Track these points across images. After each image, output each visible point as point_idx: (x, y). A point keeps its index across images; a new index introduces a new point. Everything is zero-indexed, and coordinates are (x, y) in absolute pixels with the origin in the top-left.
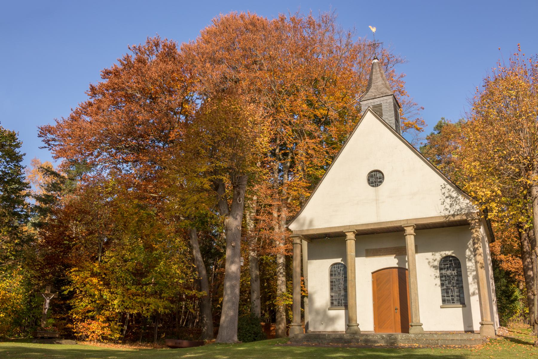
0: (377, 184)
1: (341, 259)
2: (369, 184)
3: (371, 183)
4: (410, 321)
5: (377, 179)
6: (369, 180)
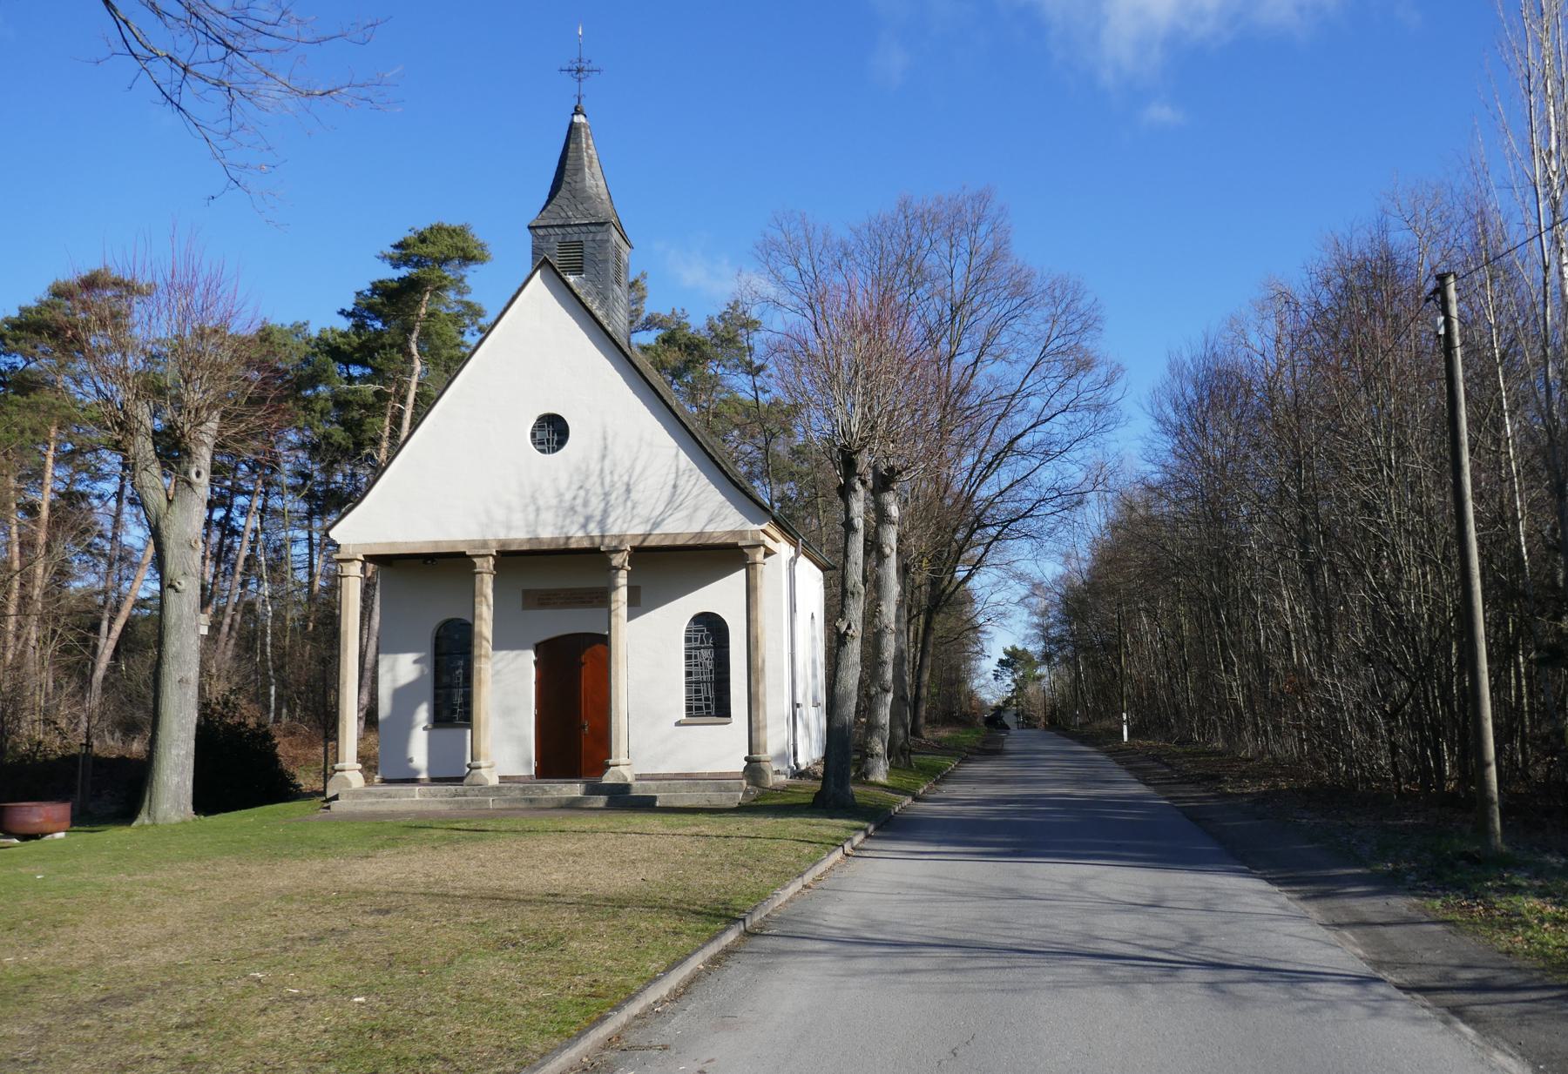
6: (533, 435)
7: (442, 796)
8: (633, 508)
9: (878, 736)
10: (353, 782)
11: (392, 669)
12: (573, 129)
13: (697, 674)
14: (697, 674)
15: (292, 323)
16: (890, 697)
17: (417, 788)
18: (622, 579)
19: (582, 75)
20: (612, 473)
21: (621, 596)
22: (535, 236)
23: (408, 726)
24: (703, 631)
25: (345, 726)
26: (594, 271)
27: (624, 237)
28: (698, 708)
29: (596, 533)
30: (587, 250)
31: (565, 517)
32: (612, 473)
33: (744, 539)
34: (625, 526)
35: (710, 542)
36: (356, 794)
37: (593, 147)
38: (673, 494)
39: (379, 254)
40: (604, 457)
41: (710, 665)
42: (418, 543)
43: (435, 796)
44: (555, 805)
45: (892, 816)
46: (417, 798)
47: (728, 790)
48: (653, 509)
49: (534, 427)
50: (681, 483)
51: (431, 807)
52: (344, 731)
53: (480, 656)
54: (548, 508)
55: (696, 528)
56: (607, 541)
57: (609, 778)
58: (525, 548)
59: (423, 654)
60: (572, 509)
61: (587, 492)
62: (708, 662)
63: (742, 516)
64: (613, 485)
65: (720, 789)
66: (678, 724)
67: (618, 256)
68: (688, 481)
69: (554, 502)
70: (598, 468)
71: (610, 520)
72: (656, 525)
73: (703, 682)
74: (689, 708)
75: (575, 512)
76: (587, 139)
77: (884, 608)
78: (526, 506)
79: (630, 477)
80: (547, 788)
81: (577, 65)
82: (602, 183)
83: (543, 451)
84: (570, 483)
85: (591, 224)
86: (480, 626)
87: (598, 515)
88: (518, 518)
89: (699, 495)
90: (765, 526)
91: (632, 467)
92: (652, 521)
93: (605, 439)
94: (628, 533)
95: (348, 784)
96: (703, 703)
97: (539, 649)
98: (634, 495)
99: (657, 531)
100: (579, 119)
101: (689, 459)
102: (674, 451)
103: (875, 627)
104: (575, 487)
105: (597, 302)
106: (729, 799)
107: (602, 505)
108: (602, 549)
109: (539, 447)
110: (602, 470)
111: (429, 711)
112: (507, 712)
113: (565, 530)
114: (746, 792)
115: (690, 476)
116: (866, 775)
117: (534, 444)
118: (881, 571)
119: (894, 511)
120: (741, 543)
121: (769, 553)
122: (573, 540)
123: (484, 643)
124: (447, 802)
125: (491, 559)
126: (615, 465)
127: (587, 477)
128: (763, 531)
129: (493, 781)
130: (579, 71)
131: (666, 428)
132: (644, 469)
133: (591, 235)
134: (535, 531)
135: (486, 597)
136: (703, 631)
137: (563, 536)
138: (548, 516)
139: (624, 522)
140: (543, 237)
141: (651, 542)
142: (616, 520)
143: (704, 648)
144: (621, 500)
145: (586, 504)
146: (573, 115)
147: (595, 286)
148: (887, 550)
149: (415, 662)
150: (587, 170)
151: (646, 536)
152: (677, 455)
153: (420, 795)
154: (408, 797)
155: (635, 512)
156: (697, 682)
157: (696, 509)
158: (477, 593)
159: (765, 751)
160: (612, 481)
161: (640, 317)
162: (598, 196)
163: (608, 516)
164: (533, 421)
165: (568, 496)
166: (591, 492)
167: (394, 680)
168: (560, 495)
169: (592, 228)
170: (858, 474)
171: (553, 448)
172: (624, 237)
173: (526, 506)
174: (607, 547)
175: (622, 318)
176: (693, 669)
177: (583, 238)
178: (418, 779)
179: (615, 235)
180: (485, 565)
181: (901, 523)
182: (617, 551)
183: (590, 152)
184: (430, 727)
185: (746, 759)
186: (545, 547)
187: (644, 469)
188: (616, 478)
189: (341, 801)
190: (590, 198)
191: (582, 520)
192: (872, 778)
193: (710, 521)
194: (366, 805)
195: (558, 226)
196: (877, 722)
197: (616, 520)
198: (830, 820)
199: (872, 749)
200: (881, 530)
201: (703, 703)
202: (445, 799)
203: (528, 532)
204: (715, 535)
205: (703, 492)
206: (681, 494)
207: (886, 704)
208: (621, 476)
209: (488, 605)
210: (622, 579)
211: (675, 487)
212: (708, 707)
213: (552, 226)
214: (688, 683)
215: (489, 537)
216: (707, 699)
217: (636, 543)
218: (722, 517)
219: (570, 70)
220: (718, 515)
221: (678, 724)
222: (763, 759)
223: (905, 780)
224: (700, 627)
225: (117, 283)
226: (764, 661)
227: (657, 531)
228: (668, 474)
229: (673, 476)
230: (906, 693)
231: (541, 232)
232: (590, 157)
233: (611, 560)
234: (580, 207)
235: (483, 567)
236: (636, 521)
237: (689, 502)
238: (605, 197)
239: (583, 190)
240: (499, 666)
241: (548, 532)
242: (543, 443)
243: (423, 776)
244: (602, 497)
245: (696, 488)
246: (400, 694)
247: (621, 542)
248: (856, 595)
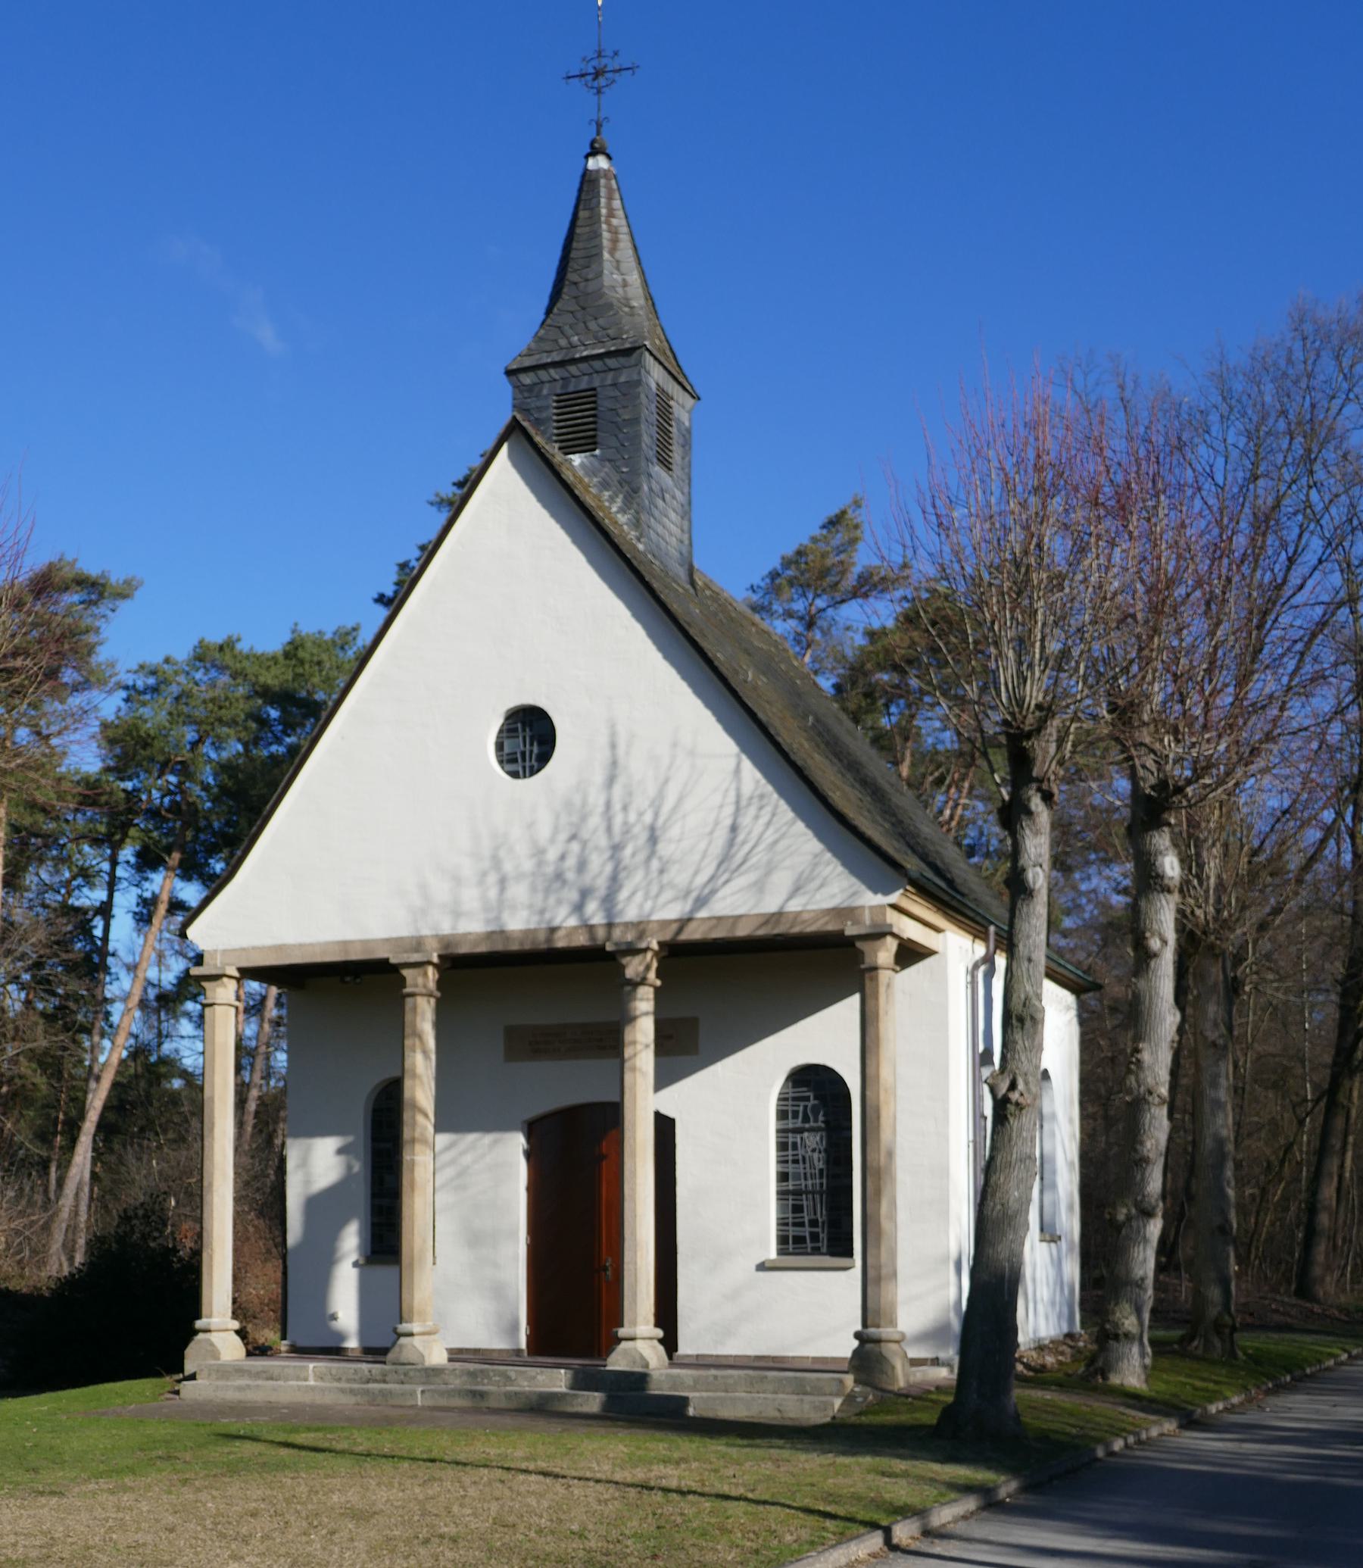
6: (499, 747)
7: (348, 1381)
8: (662, 871)
9: (1129, 1301)
10: (222, 1352)
11: (304, 1163)
12: (588, 182)
13: (797, 1177)
14: (797, 1177)
15: (334, 629)
16: (1155, 1228)
17: (311, 1366)
18: (644, 1003)
19: (602, 81)
20: (625, 808)
21: (643, 1032)
22: (518, 387)
23: (327, 1261)
24: (807, 1099)
25: (211, 1257)
26: (614, 442)
27: (678, 377)
28: (799, 1240)
29: (598, 919)
30: (604, 404)
31: (547, 891)
32: (625, 808)
33: (857, 922)
34: (648, 905)
35: (796, 930)
36: (226, 1372)
37: (621, 213)
38: (731, 843)
39: (433, 498)
40: (611, 781)
41: (819, 1162)
42: (320, 944)
43: (339, 1380)
44: (513, 1405)
45: (1097, 1460)
46: (312, 1383)
47: (818, 1391)
48: (696, 873)
49: (501, 731)
50: (746, 821)
51: (328, 1399)
52: (211, 1266)
53: (413, 1141)
54: (520, 877)
55: (770, 906)
56: (617, 933)
57: (618, 1362)
58: (483, 948)
59: (350, 1139)
60: (559, 876)
61: (584, 844)
62: (816, 1155)
63: (853, 880)
64: (627, 829)
65: (801, 1390)
66: (762, 1267)
67: (665, 411)
68: (757, 817)
69: (528, 865)
70: (601, 801)
71: (623, 895)
72: (701, 902)
73: (807, 1192)
74: (782, 1240)
75: (564, 882)
76: (610, 198)
77: (1146, 1056)
78: (484, 874)
79: (656, 815)
80: (513, 1375)
81: (595, 63)
82: (634, 278)
83: (515, 775)
84: (556, 830)
85: (609, 354)
86: (413, 1088)
87: (602, 884)
88: (470, 898)
89: (776, 842)
90: (895, 897)
91: (660, 796)
92: (694, 895)
93: (613, 746)
94: (656, 917)
95: (214, 1353)
96: (806, 1231)
97: (534, 1130)
98: (664, 849)
99: (703, 914)
100: (599, 163)
101: (758, 775)
102: (732, 763)
103: (1129, 1091)
104: (563, 836)
105: (619, 500)
106: (816, 1408)
107: (609, 868)
108: (609, 947)
109: (511, 767)
110: (608, 805)
111: (361, 1233)
112: (476, 1239)
113: (547, 916)
114: (850, 1399)
115: (761, 808)
116: (1104, 1373)
117: (501, 762)
118: (1142, 984)
119: (1171, 866)
120: (850, 930)
121: (910, 954)
122: (560, 934)
123: (420, 1118)
124: (352, 1391)
125: (430, 970)
126: (630, 794)
127: (584, 818)
128: (894, 907)
129: (436, 1356)
130: (597, 74)
131: (720, 720)
132: (680, 800)
133: (611, 375)
134: (498, 918)
135: (420, 1038)
136: (807, 1099)
137: (544, 926)
138: (519, 892)
139: (646, 897)
140: (530, 388)
141: (692, 933)
142: (633, 893)
143: (811, 1130)
144: (641, 857)
145: (582, 866)
146: (587, 157)
147: (617, 469)
148: (1155, 944)
149: (340, 1151)
150: (606, 255)
151: (684, 922)
152: (737, 771)
153: (320, 1377)
154: (298, 1379)
155: (666, 878)
156: (797, 1193)
157: (769, 870)
158: (408, 1030)
159: (893, 1322)
160: (625, 823)
161: (849, 575)
162: (626, 302)
163: (621, 887)
164: (497, 722)
165: (552, 855)
166: (590, 845)
167: (307, 1182)
168: (539, 853)
169: (611, 362)
170: (1040, 781)
171: (532, 767)
172: (678, 377)
173: (484, 874)
174: (616, 944)
175: (673, 528)
176: (791, 1168)
177: (596, 384)
178: (345, 1349)
179: (655, 375)
180: (420, 980)
181: (1184, 888)
182: (633, 951)
183: (614, 222)
184: (361, 1262)
185: (858, 1335)
186: (515, 947)
187: (680, 800)
188: (632, 817)
189: (199, 1382)
190: (610, 306)
191: (574, 896)
192: (1115, 1380)
193: (791, 896)
194: (230, 1392)
195: (555, 364)
196: (1128, 1271)
197: (633, 893)
198: (936, 1467)
199: (1116, 1325)
200: (1143, 904)
201: (806, 1231)
202: (356, 1386)
203: (488, 921)
204: (806, 916)
205: (782, 837)
206: (744, 843)
207: (1146, 1240)
208: (641, 814)
209: (425, 1052)
210: (644, 1003)
211: (734, 829)
212: (815, 1237)
213: (544, 366)
214: (782, 1194)
215: (426, 932)
216: (814, 1223)
217: (667, 936)
218: (817, 882)
219: (583, 75)
220: (810, 879)
221: (762, 1267)
222: (884, 1336)
223: (1176, 1382)
224: (804, 1092)
225: (83, 582)
226: (890, 1154)
227: (703, 914)
228: (721, 806)
229: (730, 809)
230: (1227, 1221)
231: (527, 379)
232: (614, 231)
233: (623, 967)
234: (593, 325)
235: (416, 986)
236: (668, 895)
237: (759, 857)
238: (638, 302)
239: (599, 293)
240: (467, 1159)
241: (519, 921)
242: (515, 761)
243: (352, 1343)
244: (607, 854)
245: (771, 830)
246: (314, 1204)
247: (641, 936)
248: (1028, 1023)
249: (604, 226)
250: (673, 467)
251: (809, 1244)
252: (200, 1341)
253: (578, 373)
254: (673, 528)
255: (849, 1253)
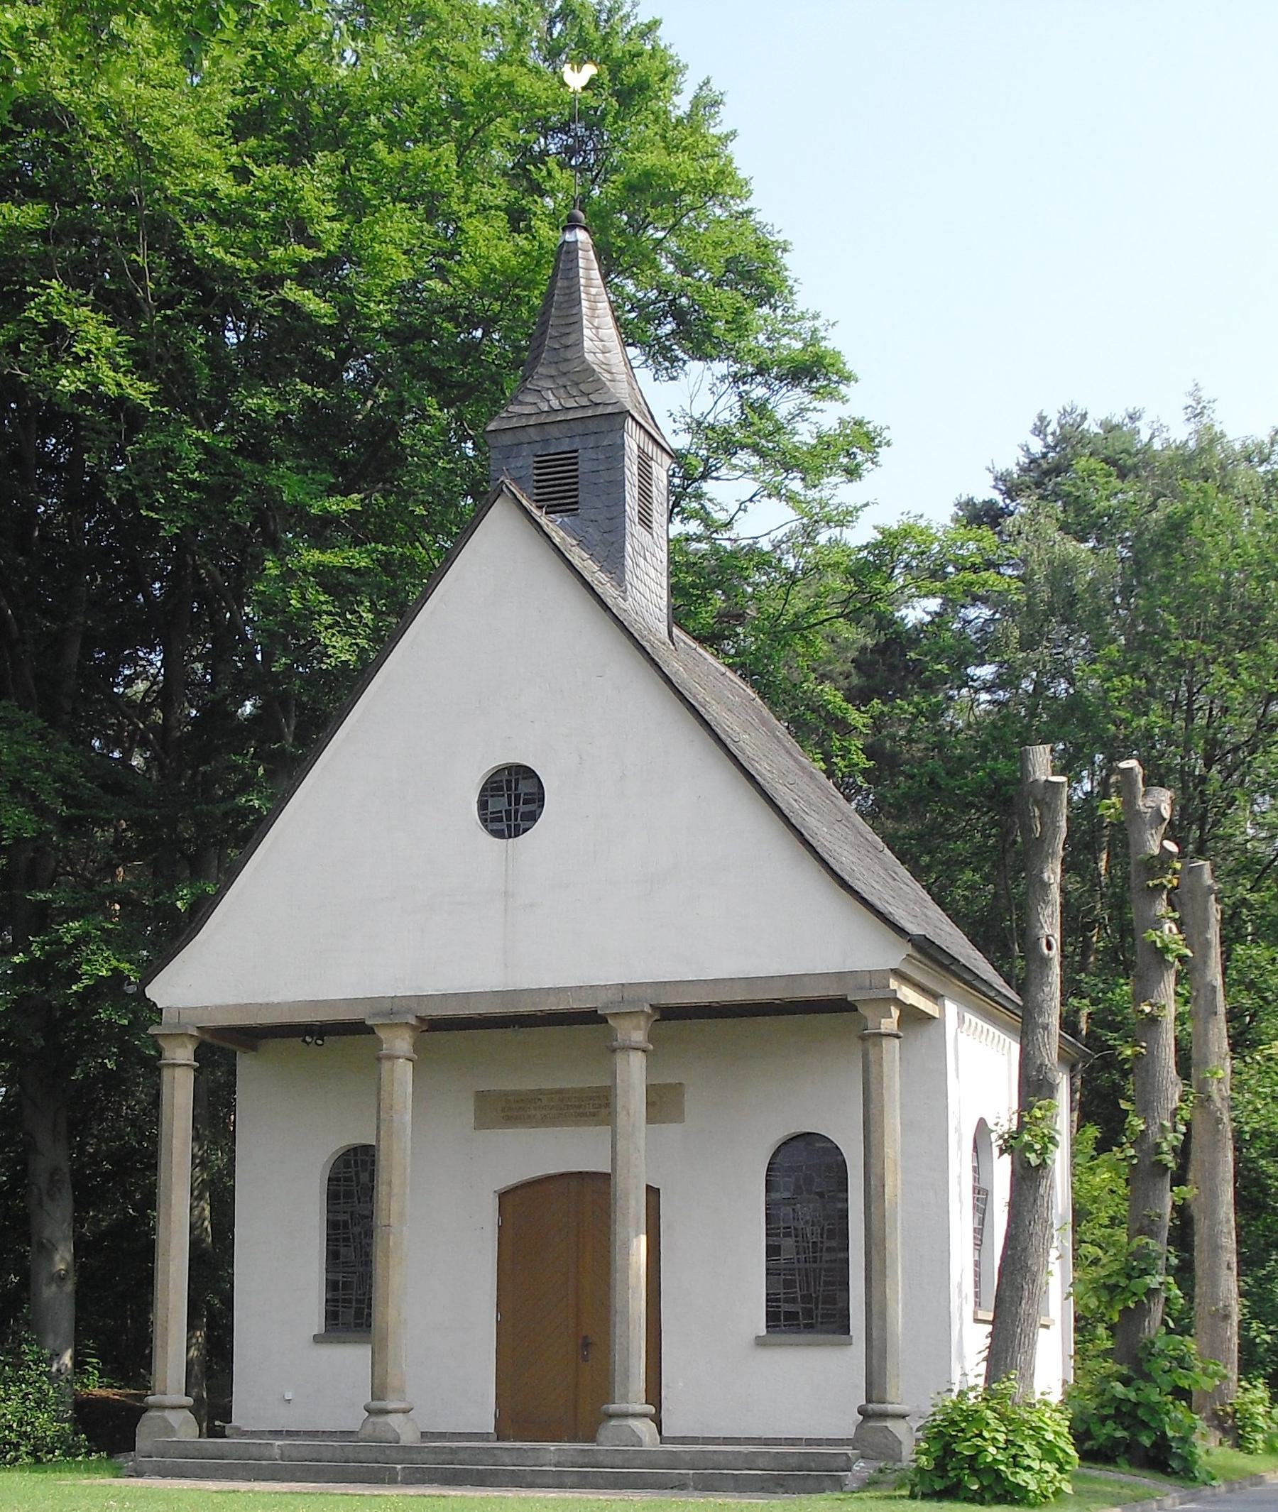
0: (517, 826)
1: (1099, 1135)
2: (484, 821)
3: (493, 820)
4: (618, 1393)
5: (517, 803)
6: (483, 805)
30: (583, 466)
83: (498, 834)
185: (861, 1411)
249: (583, 296)
250: (654, 525)
251: (802, 1321)
252: (151, 1418)
253: (558, 435)
254: (653, 586)
255: (845, 1329)
